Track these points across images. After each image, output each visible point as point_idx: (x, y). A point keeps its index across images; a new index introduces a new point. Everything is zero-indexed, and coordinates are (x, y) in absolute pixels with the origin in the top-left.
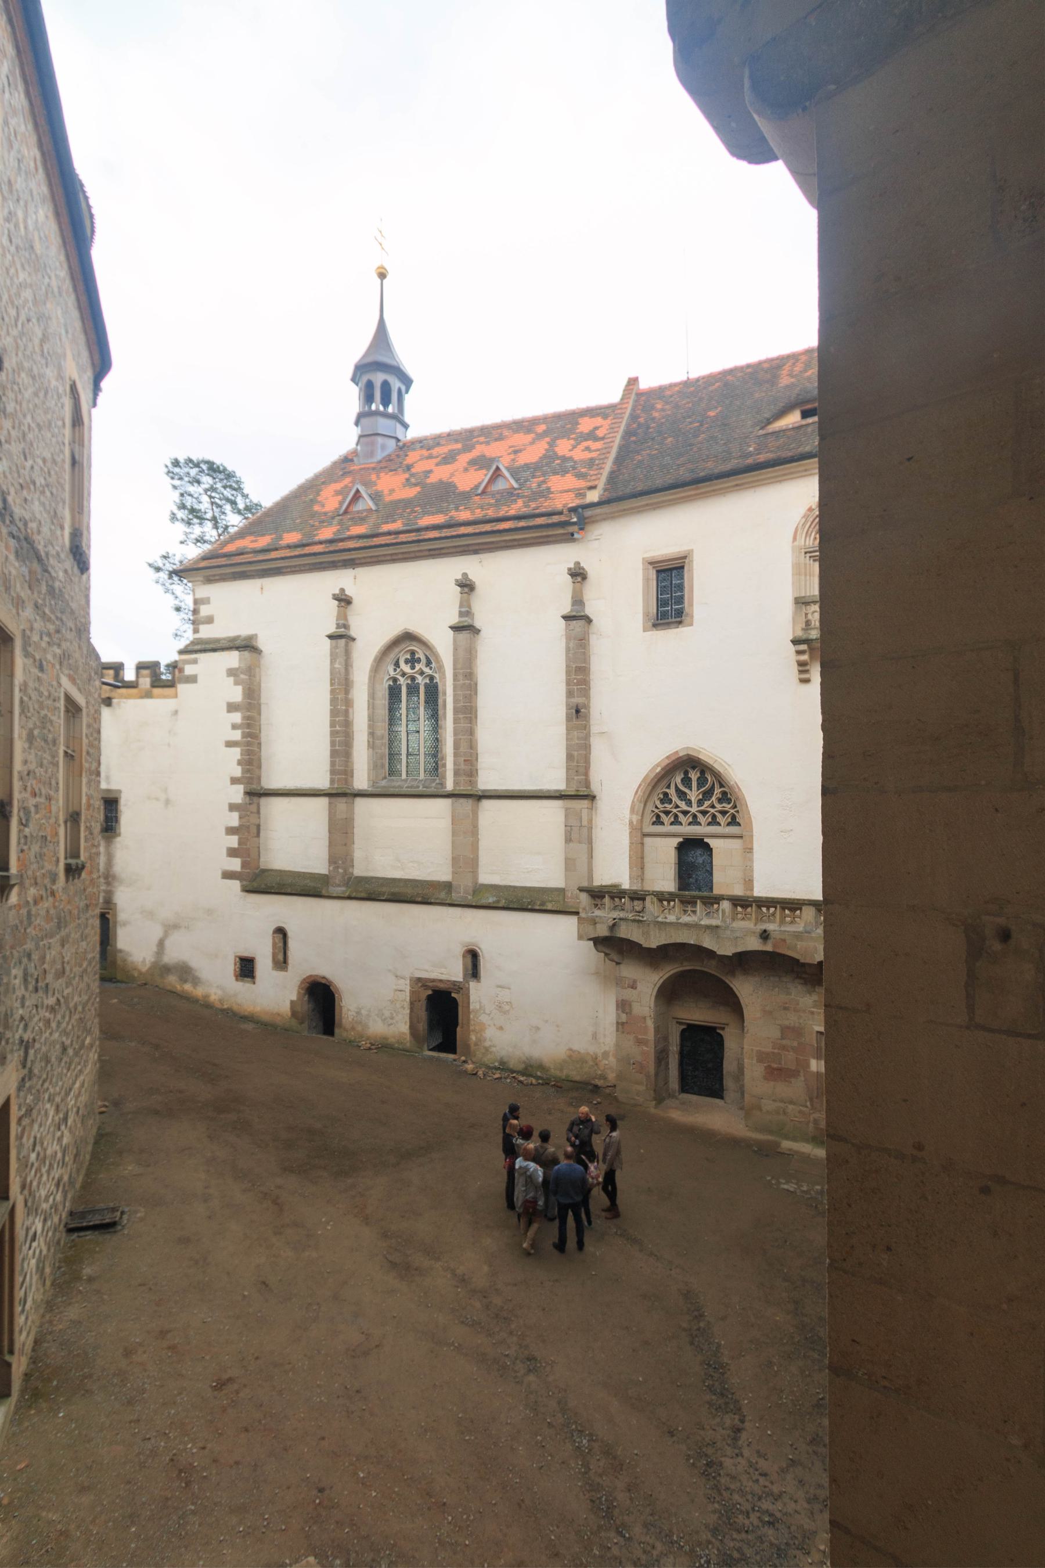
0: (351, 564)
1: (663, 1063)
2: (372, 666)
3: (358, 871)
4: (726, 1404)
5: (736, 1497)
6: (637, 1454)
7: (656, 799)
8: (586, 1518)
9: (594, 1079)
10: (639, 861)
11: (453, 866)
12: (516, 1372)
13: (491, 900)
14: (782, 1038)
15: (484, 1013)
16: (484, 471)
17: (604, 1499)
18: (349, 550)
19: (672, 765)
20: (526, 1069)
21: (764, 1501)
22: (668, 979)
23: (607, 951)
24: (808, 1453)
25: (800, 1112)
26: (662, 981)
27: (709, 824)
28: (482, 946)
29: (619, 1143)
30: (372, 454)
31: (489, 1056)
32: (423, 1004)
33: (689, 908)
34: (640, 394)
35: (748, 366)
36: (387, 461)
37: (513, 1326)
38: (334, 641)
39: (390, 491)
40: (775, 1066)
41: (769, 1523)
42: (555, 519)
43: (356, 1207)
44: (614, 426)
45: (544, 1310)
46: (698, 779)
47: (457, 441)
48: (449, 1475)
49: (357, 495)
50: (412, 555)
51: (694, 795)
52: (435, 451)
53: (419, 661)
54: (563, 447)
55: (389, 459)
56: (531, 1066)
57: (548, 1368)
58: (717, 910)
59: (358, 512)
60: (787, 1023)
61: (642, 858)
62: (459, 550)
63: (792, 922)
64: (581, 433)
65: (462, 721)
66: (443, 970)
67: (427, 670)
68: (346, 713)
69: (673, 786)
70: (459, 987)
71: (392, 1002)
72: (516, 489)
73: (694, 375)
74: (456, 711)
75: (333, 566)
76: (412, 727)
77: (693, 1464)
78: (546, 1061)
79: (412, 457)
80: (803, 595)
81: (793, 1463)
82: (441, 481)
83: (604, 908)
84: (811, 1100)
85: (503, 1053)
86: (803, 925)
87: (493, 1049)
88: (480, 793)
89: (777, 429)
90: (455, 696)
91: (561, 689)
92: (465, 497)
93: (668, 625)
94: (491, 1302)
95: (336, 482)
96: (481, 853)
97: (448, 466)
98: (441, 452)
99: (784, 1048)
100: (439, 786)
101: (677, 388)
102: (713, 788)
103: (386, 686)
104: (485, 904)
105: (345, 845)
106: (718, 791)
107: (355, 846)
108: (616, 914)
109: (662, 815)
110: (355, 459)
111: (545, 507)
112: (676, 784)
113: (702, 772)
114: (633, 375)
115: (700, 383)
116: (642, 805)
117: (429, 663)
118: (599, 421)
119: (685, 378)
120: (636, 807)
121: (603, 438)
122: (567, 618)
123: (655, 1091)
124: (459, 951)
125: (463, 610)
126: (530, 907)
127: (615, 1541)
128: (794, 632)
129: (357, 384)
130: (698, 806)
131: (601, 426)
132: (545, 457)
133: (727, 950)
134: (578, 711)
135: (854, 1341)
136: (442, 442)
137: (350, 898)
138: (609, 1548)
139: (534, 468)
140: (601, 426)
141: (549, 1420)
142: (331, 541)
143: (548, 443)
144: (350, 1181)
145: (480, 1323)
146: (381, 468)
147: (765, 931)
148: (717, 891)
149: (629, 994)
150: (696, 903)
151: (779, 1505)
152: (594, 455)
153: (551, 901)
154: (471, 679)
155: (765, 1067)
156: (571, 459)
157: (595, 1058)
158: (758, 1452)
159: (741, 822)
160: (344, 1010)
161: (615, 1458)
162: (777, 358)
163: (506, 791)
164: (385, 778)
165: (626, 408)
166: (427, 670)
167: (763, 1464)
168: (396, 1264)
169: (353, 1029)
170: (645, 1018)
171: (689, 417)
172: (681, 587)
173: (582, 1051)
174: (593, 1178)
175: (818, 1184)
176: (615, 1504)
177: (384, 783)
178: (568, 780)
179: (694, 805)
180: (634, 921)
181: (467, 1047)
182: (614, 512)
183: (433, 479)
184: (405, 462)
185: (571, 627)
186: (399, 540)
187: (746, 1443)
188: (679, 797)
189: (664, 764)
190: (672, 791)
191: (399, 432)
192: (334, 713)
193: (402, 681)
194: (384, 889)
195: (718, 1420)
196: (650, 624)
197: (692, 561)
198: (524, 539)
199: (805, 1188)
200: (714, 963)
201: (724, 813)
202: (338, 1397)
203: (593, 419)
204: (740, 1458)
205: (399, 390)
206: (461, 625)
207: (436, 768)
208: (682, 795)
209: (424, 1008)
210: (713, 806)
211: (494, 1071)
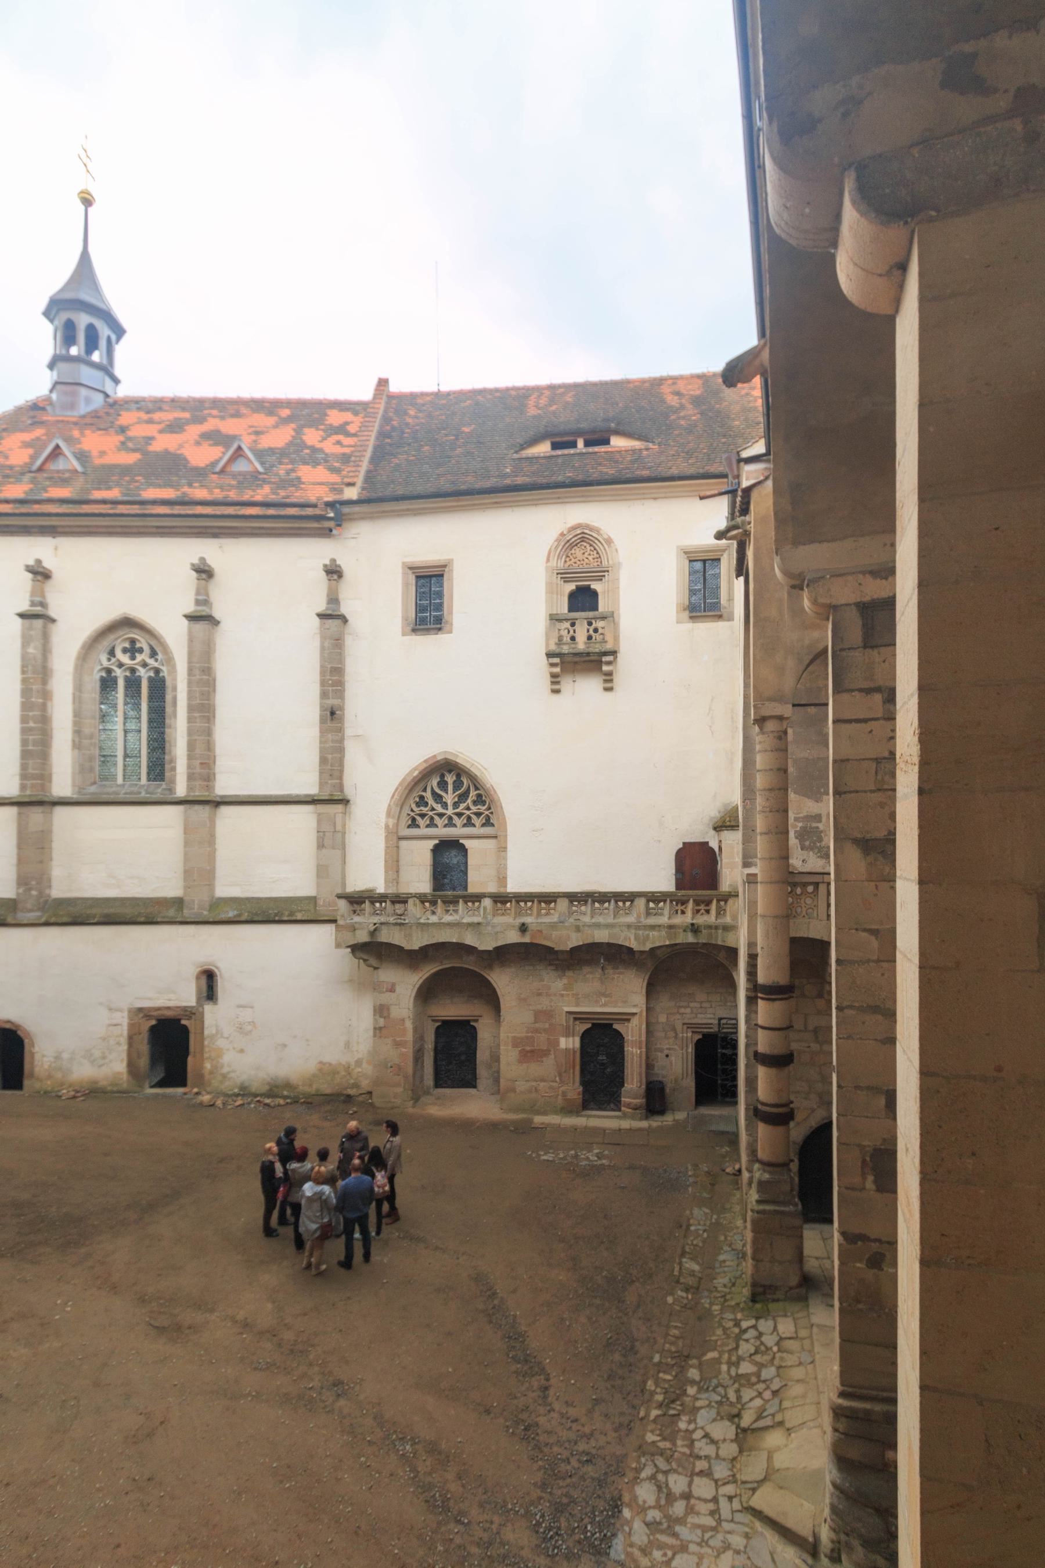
0: (52, 531)
1: (420, 1061)
2: (79, 653)
3: (57, 892)
4: (531, 1368)
5: (556, 1449)
6: (460, 1442)
7: (412, 802)
8: (425, 1520)
9: (346, 1089)
10: (394, 865)
11: (185, 880)
12: (324, 1401)
13: (231, 914)
14: (536, 1022)
15: (222, 1037)
16: (221, 449)
17: (437, 1495)
18: (50, 515)
19: (429, 769)
20: (271, 1090)
21: (579, 1444)
22: (427, 979)
23: (366, 957)
24: (607, 1389)
25: (551, 1087)
26: (421, 981)
27: (464, 825)
28: (219, 965)
29: (400, 1147)
30: (72, 406)
31: (227, 1083)
32: (145, 1036)
33: (451, 908)
34: (391, 397)
35: (497, 390)
36: (92, 417)
37: (311, 1357)
38: (27, 622)
39: (100, 452)
40: (528, 1048)
41: (587, 1461)
42: (309, 511)
43: (98, 1277)
44: (367, 424)
45: (341, 1331)
46: (454, 782)
47: (184, 409)
48: (275, 1530)
49: (56, 452)
50: (135, 530)
51: (450, 798)
52: (157, 416)
53: (141, 651)
54: (312, 437)
55: (95, 415)
56: (277, 1087)
57: (357, 1388)
58: (479, 908)
59: (58, 471)
60: (539, 1007)
61: (398, 861)
62: (196, 530)
63: (547, 914)
64: (331, 425)
65: (198, 720)
66: (172, 996)
67: (151, 662)
68: (44, 707)
69: (429, 790)
70: (190, 1013)
71: (104, 1039)
72: (260, 473)
73: (444, 388)
74: (191, 709)
75: (25, 531)
76: (132, 725)
77: (513, 1433)
78: (294, 1079)
79: (126, 418)
80: (555, 612)
81: (597, 1402)
82: (167, 452)
83: (364, 914)
84: (560, 1075)
85: (244, 1077)
86: (557, 916)
87: (232, 1075)
88: (218, 799)
89: (530, 455)
90: (190, 692)
91: (316, 690)
92: (200, 474)
93: (427, 631)
94: (282, 1339)
95: (22, 431)
96: (219, 863)
97: (174, 435)
98: (164, 418)
99: (537, 1031)
100: (167, 792)
101: (428, 398)
102: (467, 792)
103: (97, 677)
104: (224, 919)
105: (41, 862)
106: (473, 794)
107: (54, 863)
108: (376, 919)
109: (418, 818)
110: (49, 408)
111: (296, 497)
112: (432, 788)
113: (458, 776)
114: (383, 376)
115: (451, 397)
116: (399, 809)
117: (153, 654)
118: (348, 416)
119: (435, 389)
120: (393, 811)
121: (355, 435)
122: (322, 616)
123: (412, 1090)
124: (192, 972)
125: (200, 598)
126: (277, 918)
127: (456, 1530)
128: (547, 645)
129: (52, 321)
130: (454, 809)
131: (352, 422)
132: (290, 444)
133: (486, 944)
134: (332, 713)
135: (943, 1235)
136: (165, 407)
137: (47, 924)
138: (451, 1540)
139: (282, 454)
140: (352, 422)
141: (369, 1439)
142: (22, 502)
143: (294, 430)
144: (83, 1250)
145: (275, 1364)
146: (86, 424)
147: (523, 924)
148: (472, 889)
149: (386, 998)
150: (458, 902)
151: (593, 1443)
152: (347, 450)
153: (301, 911)
154: (209, 675)
155: (520, 1052)
156: (321, 450)
157: (348, 1069)
158: (567, 1402)
159: (495, 823)
160: (37, 1057)
161: (440, 1453)
162: (524, 388)
163: (249, 796)
164: (95, 783)
165: (379, 408)
166: (151, 662)
167: (572, 1412)
168: (164, 1328)
169: (50, 1077)
170: (403, 1020)
171: (444, 429)
172: (440, 595)
173: (334, 1062)
174: (379, 1187)
175: (572, 1149)
176: (449, 1496)
177: (93, 789)
178: (322, 784)
179: (450, 807)
180: (396, 924)
181: (201, 1076)
182: (372, 513)
183: (157, 446)
184: (118, 423)
185: (327, 626)
186: (117, 511)
187: (555, 1398)
188: (435, 800)
189: (421, 768)
190: (428, 795)
191: (109, 386)
192: (26, 706)
193: (118, 672)
194: (94, 911)
195: (527, 1385)
196: (409, 628)
197: (452, 570)
198: (273, 528)
199: (561, 1156)
200: (472, 958)
201: (478, 814)
202: (127, 1493)
203: (342, 413)
204: (552, 1413)
205: (109, 339)
206: (199, 614)
207: (159, 769)
208: (438, 798)
209: (146, 1041)
210: (468, 808)
211: (235, 1098)
